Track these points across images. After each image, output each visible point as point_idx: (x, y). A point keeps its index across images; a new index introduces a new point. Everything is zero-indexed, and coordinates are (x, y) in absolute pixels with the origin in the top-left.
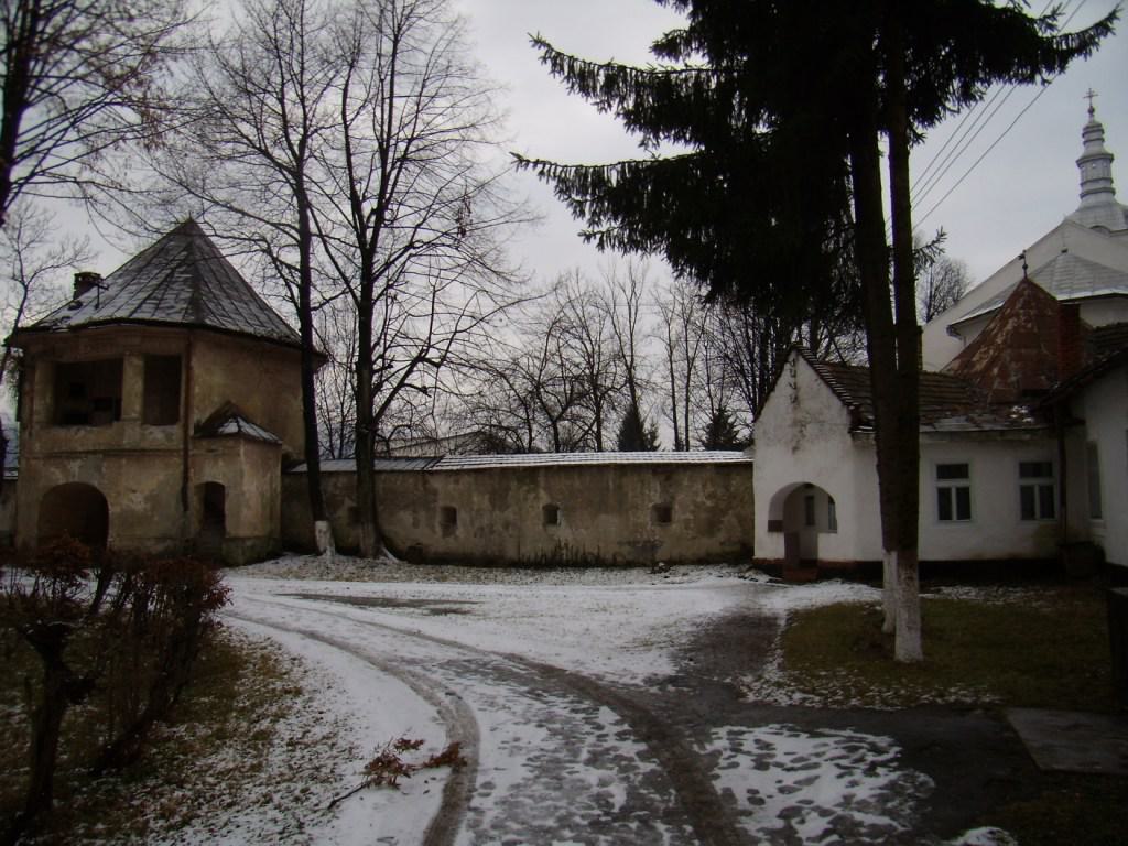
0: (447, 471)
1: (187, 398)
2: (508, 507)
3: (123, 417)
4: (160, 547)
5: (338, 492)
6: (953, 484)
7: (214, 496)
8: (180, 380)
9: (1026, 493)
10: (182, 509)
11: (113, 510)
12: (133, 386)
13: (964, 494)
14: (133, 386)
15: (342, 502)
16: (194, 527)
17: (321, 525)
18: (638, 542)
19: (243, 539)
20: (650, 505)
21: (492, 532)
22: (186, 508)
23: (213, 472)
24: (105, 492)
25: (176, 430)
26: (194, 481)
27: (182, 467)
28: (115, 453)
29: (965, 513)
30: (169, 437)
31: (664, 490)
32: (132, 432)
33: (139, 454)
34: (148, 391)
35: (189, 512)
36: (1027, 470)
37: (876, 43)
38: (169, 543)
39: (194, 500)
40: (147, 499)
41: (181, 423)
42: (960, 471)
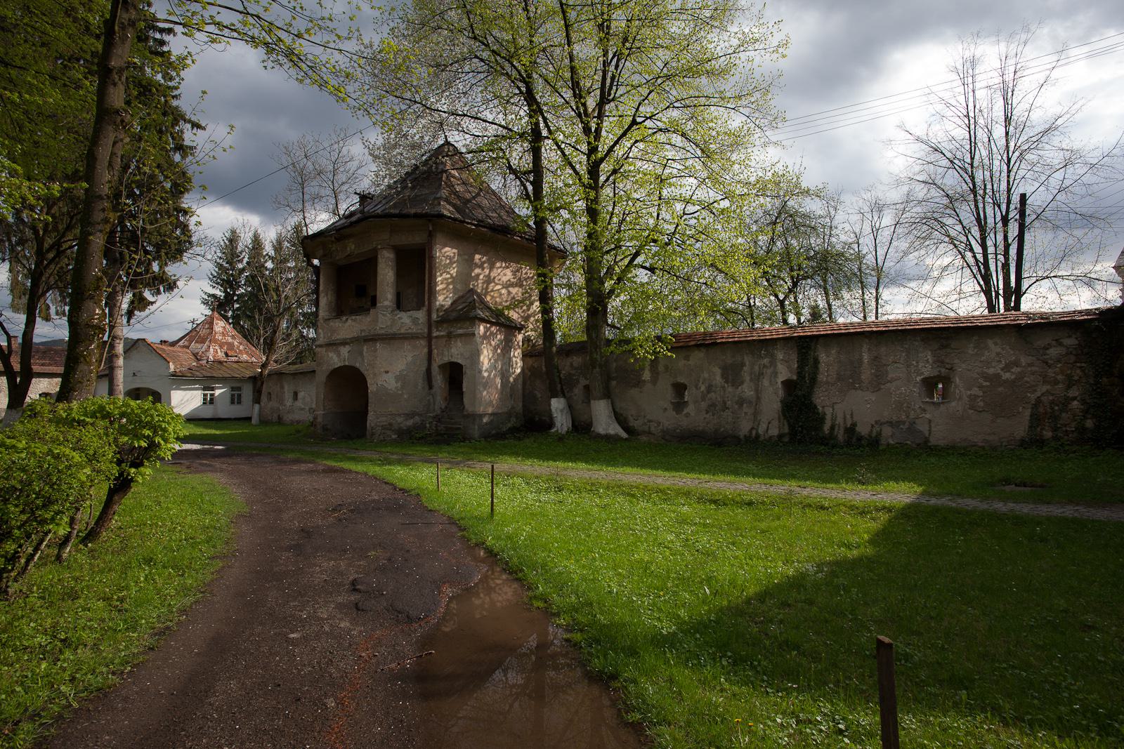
0: (823, 335)
1: (430, 284)
2: (742, 383)
3: (378, 305)
4: (410, 423)
5: (573, 372)
6: (236, 393)
7: (455, 374)
8: (425, 268)
9: (233, 396)
10: (427, 387)
11: (372, 388)
12: (386, 275)
13: (239, 396)
14: (386, 275)
15: (578, 382)
16: (440, 401)
17: (557, 404)
18: (904, 423)
19: (481, 416)
20: (919, 379)
21: (725, 408)
22: (431, 387)
23: (456, 353)
24: (365, 373)
25: (421, 315)
26: (438, 360)
27: (426, 350)
28: (371, 339)
29: (239, 402)
30: (415, 321)
31: (939, 362)
32: (385, 317)
33: (390, 338)
34: (399, 275)
35: (434, 390)
36: (233, 389)
37: (18, 380)
38: (417, 419)
39: (439, 380)
40: (397, 378)
41: (425, 309)
42: (239, 389)
